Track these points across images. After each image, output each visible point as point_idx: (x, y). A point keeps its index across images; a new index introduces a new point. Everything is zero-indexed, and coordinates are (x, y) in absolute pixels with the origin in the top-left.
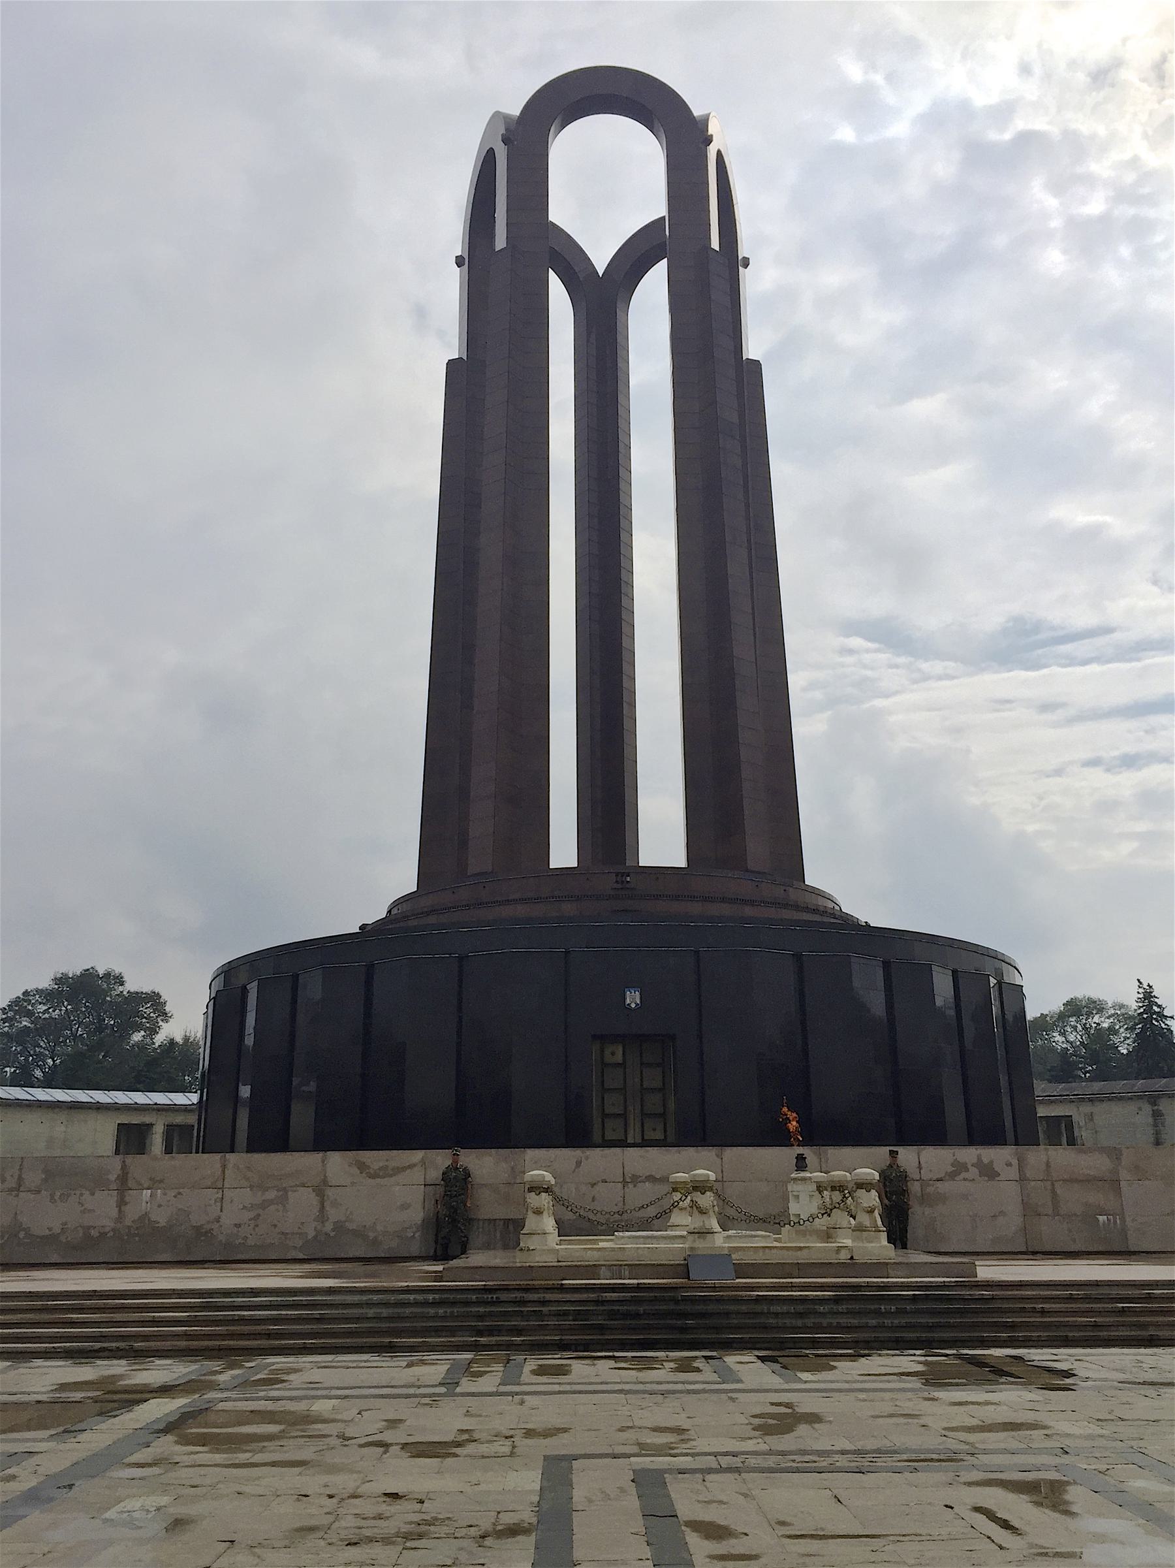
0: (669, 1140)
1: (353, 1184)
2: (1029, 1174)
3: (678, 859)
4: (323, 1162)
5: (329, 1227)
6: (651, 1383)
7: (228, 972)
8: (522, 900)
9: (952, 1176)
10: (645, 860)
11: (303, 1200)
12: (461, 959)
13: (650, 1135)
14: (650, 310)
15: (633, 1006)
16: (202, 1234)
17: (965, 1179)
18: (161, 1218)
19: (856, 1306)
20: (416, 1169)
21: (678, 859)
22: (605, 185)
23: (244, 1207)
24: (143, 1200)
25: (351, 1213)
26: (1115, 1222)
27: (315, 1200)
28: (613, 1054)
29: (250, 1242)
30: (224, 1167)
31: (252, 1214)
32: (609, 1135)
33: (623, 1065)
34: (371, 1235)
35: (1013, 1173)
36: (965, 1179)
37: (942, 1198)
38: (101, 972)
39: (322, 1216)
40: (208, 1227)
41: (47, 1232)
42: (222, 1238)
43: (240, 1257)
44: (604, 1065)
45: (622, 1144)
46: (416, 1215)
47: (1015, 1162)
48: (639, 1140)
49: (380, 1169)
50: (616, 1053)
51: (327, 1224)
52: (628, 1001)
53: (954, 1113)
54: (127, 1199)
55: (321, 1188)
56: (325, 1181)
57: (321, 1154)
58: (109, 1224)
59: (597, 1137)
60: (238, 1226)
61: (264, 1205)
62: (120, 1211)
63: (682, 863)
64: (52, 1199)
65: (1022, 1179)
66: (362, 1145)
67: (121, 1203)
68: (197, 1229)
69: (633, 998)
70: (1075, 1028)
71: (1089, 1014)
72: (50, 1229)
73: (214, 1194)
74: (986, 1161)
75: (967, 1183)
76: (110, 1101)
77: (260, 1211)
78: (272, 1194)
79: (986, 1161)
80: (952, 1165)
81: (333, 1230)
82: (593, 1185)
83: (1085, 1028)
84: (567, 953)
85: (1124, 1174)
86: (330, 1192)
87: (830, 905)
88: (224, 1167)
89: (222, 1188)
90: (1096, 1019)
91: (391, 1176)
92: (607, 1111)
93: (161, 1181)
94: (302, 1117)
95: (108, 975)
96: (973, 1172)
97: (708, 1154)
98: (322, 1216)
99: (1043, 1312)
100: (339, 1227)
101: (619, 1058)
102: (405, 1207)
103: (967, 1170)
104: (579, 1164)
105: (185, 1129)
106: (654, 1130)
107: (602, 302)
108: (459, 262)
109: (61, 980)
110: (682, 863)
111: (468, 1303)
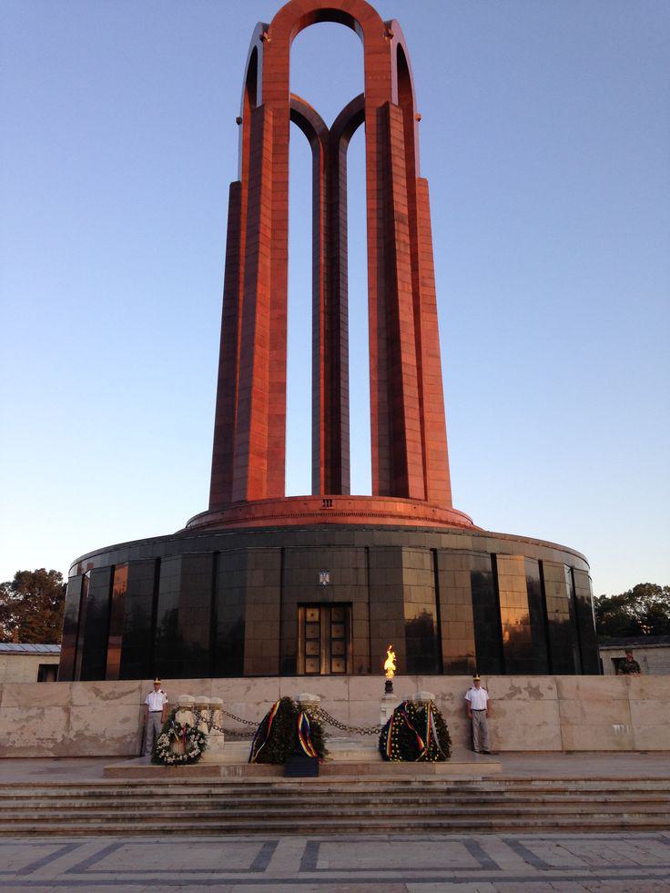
0: (322, 673)
1: (90, 703)
2: (565, 695)
3: (308, 491)
4: (70, 688)
5: (72, 734)
7: (79, 563)
8: (264, 518)
9: (510, 696)
11: (55, 718)
12: (217, 554)
13: (335, 669)
14: (357, 151)
15: (324, 583)
17: (519, 699)
19: (402, 798)
20: (135, 694)
21: (308, 491)
22: (327, 71)
23: (15, 720)
25: (89, 725)
26: (626, 730)
27: (63, 715)
28: (312, 615)
29: (17, 745)
31: (19, 726)
32: (309, 670)
35: (554, 694)
36: (519, 699)
37: (504, 713)
38: (48, 571)
43: (7, 755)
44: (306, 623)
47: (555, 687)
48: (303, 673)
49: (111, 693)
50: (313, 615)
51: (71, 732)
53: (260, 635)
56: (71, 702)
59: (300, 671)
60: (9, 734)
61: (29, 719)
63: (371, 495)
65: (560, 698)
69: (325, 578)
70: (640, 603)
71: (650, 595)
75: (521, 702)
76: (34, 650)
77: (24, 723)
78: (33, 712)
80: (510, 689)
81: (75, 737)
82: (258, 704)
83: (647, 604)
85: (631, 695)
86: (74, 711)
87: (463, 521)
90: (654, 598)
91: (117, 698)
92: (308, 653)
94: (114, 657)
95: (52, 572)
96: (525, 694)
99: (544, 803)
100: (79, 734)
101: (316, 618)
102: (126, 720)
103: (521, 692)
104: (249, 688)
105: (54, 667)
107: (329, 147)
108: (239, 121)
109: (20, 576)
110: (371, 495)
111: (109, 796)
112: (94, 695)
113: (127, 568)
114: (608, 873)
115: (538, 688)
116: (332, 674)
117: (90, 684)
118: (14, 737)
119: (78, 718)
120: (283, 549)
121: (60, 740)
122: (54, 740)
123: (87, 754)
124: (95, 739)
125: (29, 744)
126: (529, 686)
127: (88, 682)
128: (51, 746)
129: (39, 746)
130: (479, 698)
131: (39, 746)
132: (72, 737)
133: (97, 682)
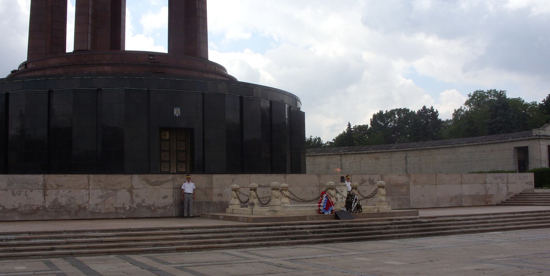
3: (161, 46)
5: (135, 205)
6: (186, 263)
10: (127, 49)
12: (7, 95)
16: (82, 208)
18: (63, 201)
21: (161, 46)
24: (52, 195)
27: (128, 194)
28: (165, 135)
30: (89, 180)
33: (169, 140)
34: (153, 208)
39: (132, 201)
40: (84, 205)
41: (13, 208)
42: (90, 209)
43: (98, 217)
45: (168, 173)
46: (170, 200)
48: (175, 171)
52: (175, 113)
54: (47, 193)
55: (130, 190)
56: (132, 187)
57: (130, 176)
58: (40, 204)
60: (97, 205)
62: (45, 199)
63: (67, 52)
64: (13, 194)
66: (149, 172)
67: (45, 195)
68: (79, 206)
69: (177, 112)
72: (14, 206)
73: (84, 192)
74: (372, 179)
79: (372, 179)
84: (149, 90)
85: (411, 183)
86: (135, 192)
88: (89, 180)
89: (89, 189)
93: (62, 186)
96: (368, 183)
97: (280, 177)
98: (132, 201)
100: (139, 205)
101: (167, 137)
102: (165, 197)
104: (233, 181)
106: (182, 167)
110: (67, 52)
112: (145, 183)
113: (105, 193)
114: (49, 272)
115: (373, 180)
116: (178, 173)
117: (143, 176)
118: (100, 207)
119: (137, 196)
120: (50, 92)
121: (128, 208)
122: (124, 208)
123: (145, 216)
124: (149, 207)
125: (110, 211)
126: (370, 178)
127: (142, 175)
128: (123, 212)
129: (116, 212)
130: (189, 187)
131: (116, 212)
132: (135, 207)
133: (147, 175)
